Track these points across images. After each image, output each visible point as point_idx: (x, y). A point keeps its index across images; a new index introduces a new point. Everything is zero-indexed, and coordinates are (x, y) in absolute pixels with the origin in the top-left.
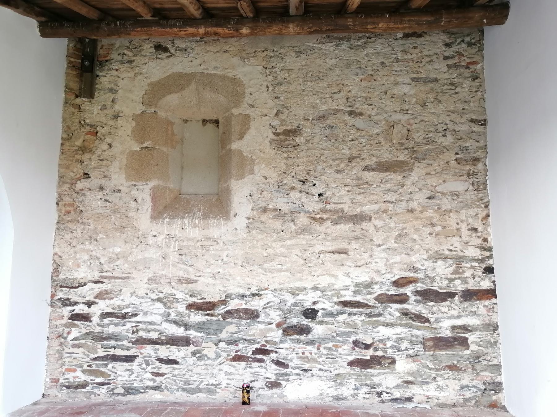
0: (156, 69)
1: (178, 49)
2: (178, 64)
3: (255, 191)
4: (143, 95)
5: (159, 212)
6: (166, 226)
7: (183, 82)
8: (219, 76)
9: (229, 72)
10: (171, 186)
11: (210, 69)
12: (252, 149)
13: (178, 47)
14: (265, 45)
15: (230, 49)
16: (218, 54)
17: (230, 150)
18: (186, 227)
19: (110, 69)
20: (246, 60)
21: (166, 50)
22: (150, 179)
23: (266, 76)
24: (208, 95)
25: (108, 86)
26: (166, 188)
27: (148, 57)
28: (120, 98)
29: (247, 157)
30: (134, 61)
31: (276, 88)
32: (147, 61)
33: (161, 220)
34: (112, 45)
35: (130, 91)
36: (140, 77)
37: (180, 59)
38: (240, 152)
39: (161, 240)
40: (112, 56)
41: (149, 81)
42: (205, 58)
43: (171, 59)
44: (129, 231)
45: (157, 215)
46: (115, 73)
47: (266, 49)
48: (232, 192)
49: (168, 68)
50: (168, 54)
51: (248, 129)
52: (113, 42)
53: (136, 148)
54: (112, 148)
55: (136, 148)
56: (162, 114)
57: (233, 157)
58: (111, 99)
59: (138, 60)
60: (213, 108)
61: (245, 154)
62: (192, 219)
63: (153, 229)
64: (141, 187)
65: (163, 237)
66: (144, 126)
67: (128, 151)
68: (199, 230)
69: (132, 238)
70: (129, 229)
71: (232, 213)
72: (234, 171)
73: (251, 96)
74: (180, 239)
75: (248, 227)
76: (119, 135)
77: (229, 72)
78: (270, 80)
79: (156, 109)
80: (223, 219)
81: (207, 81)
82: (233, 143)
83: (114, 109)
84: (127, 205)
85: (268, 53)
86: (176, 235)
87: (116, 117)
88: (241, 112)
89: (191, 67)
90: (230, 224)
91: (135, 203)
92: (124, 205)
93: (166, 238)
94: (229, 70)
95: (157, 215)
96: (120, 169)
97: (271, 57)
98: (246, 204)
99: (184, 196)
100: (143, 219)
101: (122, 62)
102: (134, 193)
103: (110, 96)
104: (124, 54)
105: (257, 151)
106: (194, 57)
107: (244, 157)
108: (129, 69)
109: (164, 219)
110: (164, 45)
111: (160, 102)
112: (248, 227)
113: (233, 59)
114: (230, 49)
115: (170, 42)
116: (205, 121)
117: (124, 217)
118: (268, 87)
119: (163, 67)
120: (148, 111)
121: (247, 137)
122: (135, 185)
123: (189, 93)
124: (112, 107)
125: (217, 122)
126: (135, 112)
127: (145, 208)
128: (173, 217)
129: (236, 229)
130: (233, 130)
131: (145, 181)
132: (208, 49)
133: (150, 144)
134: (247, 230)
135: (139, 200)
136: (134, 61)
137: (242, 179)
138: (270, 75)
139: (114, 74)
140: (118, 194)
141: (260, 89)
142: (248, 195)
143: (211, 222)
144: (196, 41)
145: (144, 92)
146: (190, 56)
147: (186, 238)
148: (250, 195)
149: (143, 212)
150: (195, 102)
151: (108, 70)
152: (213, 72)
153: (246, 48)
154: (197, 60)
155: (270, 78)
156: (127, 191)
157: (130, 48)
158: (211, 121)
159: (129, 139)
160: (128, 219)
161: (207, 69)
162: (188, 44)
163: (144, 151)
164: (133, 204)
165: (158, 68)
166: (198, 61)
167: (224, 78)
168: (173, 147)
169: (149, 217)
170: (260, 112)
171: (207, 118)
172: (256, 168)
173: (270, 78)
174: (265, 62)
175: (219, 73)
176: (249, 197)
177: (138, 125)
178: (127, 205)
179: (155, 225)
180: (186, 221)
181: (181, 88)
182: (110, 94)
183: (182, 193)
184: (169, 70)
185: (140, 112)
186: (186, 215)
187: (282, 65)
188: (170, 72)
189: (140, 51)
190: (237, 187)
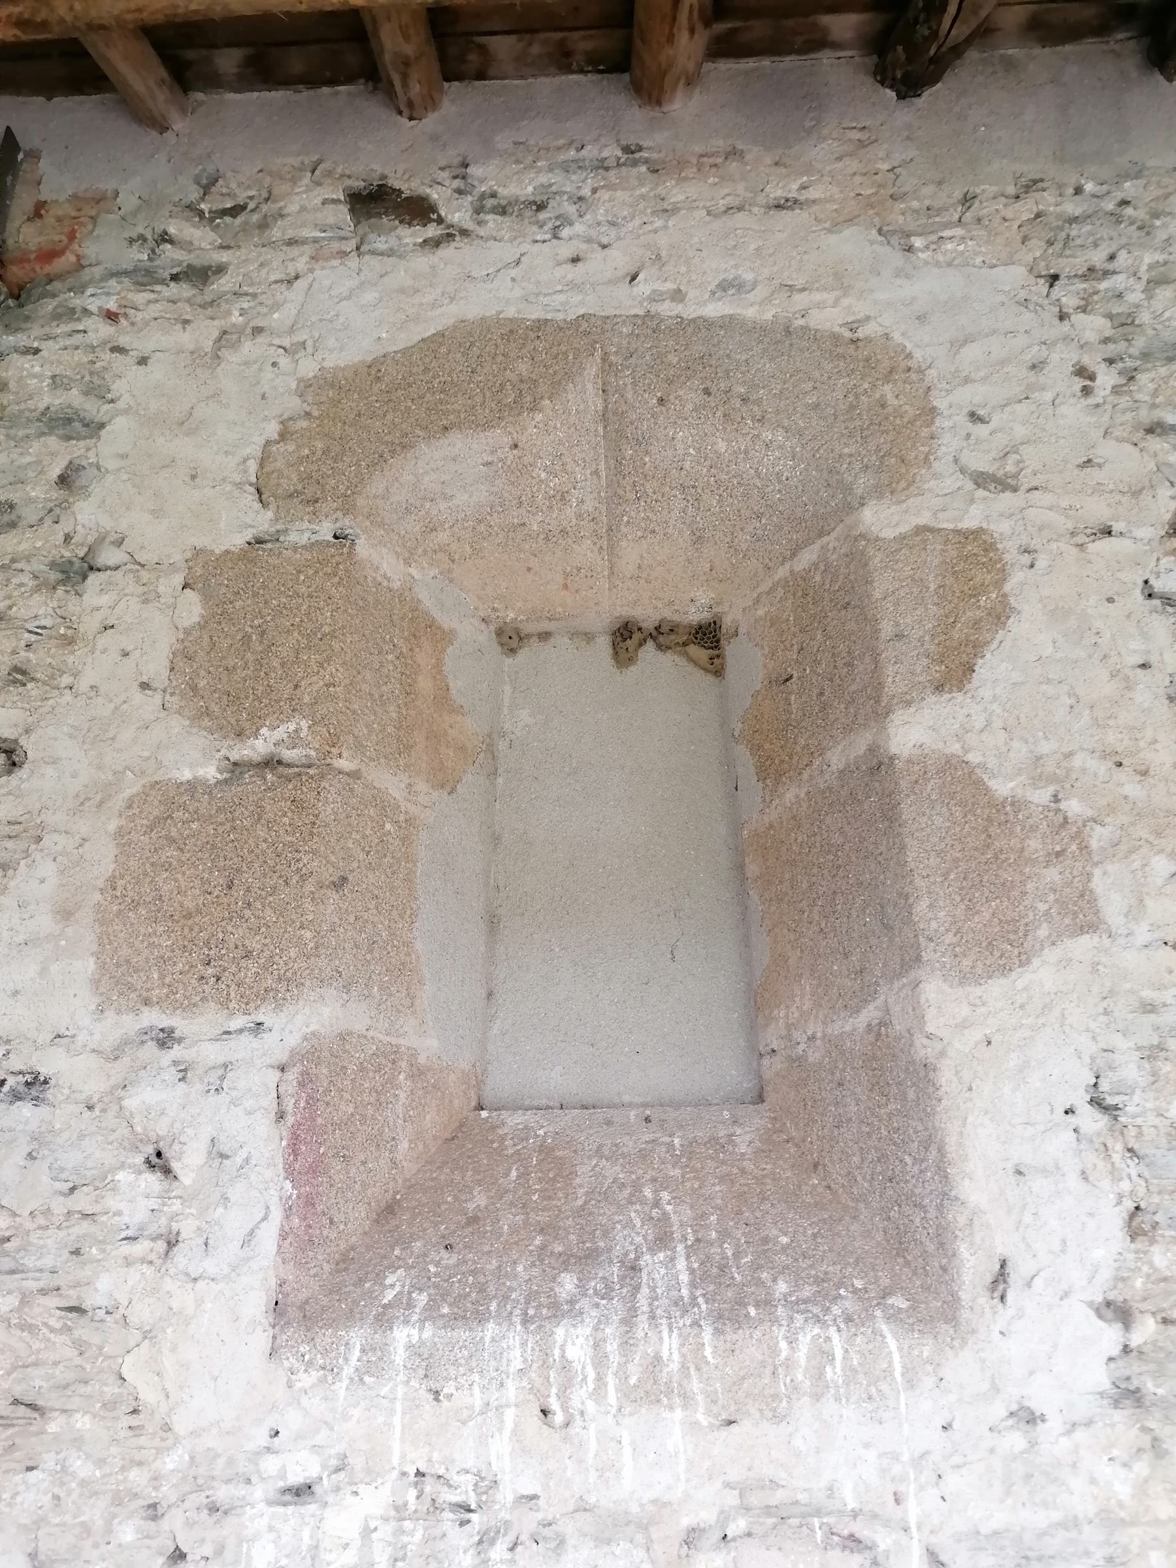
0: (359, 304)
1: (490, 203)
2: (492, 278)
3: (1131, 1071)
4: (268, 443)
5: (344, 1261)
6: (399, 1386)
7: (523, 367)
8: (760, 331)
9: (820, 306)
10: (427, 1045)
11: (692, 294)
12: (1045, 748)
13: (494, 195)
14: (1019, 168)
15: (813, 193)
16: (740, 218)
17: (878, 765)
18: (580, 1396)
19: (70, 314)
20: (918, 242)
21: (418, 210)
22: (280, 987)
23: (1062, 317)
24: (684, 441)
25: (46, 400)
26: (393, 1055)
27: (308, 249)
28: (110, 464)
29: (1017, 804)
30: (221, 269)
31: (1143, 378)
32: (301, 265)
33: (357, 1337)
34: (99, 199)
35: (187, 424)
36: (249, 349)
37: (505, 251)
38: (959, 779)
39: (352, 1532)
40: (90, 249)
41: (308, 368)
42: (663, 240)
43: (447, 252)
44: (78, 1441)
45: (317, 1303)
46: (100, 330)
47: (1032, 185)
48: (946, 1077)
49: (428, 298)
50: (432, 231)
51: (1001, 615)
52: (108, 186)
53: (196, 761)
54: (23, 773)
55: (196, 761)
56: (379, 558)
57: (907, 810)
58: (56, 471)
59: (245, 264)
60: (698, 540)
61: (1002, 787)
62: (629, 1322)
63: (291, 1421)
64: (211, 1053)
65: (373, 1501)
66: (256, 630)
67: (132, 787)
68: (692, 1426)
69: (95, 1513)
70: (83, 1422)
71: (972, 1269)
72: (933, 913)
73: (981, 430)
74: (528, 1522)
75: (1128, 1395)
76: (83, 685)
77: (820, 306)
78: (1091, 336)
79: (346, 523)
80: (893, 1317)
81: (681, 357)
82: (899, 716)
83: (65, 526)
84: (82, 1201)
85: (1047, 200)
86: (488, 1484)
87: (76, 571)
88: (925, 519)
89: (573, 286)
90: (962, 1367)
91: (152, 1180)
92: (59, 1206)
93: (399, 1509)
94: (817, 296)
95: (317, 1303)
96: (65, 914)
97: (1074, 220)
98: (1073, 1181)
99: (514, 1120)
100: (207, 1336)
101: (145, 277)
102: (156, 1099)
103: (56, 454)
104: (165, 238)
105: (1092, 764)
106: (589, 241)
107: (999, 806)
108: (187, 311)
109: (384, 1320)
110: (408, 186)
111: (377, 485)
112: (1128, 1395)
113: (833, 238)
114: (813, 193)
115: (445, 174)
116: (626, 637)
117: (46, 1310)
118: (1082, 372)
119: (402, 291)
120: (293, 537)
121: (993, 670)
122: (166, 1039)
123: (563, 432)
124: (55, 513)
125: (709, 635)
126: (202, 541)
127: (234, 1222)
128: (464, 1305)
129: (1030, 1418)
130: (887, 629)
131: (247, 1003)
132: (677, 196)
133: (294, 740)
134: (1122, 1427)
135: (189, 1162)
136: (221, 269)
137: (1005, 970)
138: (1084, 310)
139: (92, 338)
140: (25, 1109)
141: (1031, 387)
142: (1080, 1099)
143: (799, 1343)
144: (602, 166)
145: (272, 429)
146: (565, 232)
147: (583, 1508)
148: (1096, 1102)
149: (210, 1266)
150: (589, 505)
151: (57, 317)
152: (714, 310)
153: (908, 182)
154: (612, 253)
155: (1093, 326)
156: (94, 1087)
157: (201, 214)
158: (662, 635)
159: (150, 704)
160: (83, 1330)
161: (678, 296)
162: (556, 179)
163: (251, 783)
164: (135, 1196)
165: (370, 296)
166: (619, 259)
167: (784, 336)
168: (447, 783)
169: (256, 1304)
170: (1066, 511)
171: (647, 614)
172: (1110, 889)
173: (1093, 326)
174: (1037, 248)
175: (750, 313)
176: (1092, 1121)
177: (219, 614)
178: (82, 1201)
179: (306, 1380)
180: (574, 1341)
181: (514, 401)
182: (52, 442)
183: (489, 1095)
184: (434, 305)
185: (238, 541)
186: (568, 1283)
187: (1148, 258)
188: (444, 317)
189: (264, 225)
190: (977, 1035)
